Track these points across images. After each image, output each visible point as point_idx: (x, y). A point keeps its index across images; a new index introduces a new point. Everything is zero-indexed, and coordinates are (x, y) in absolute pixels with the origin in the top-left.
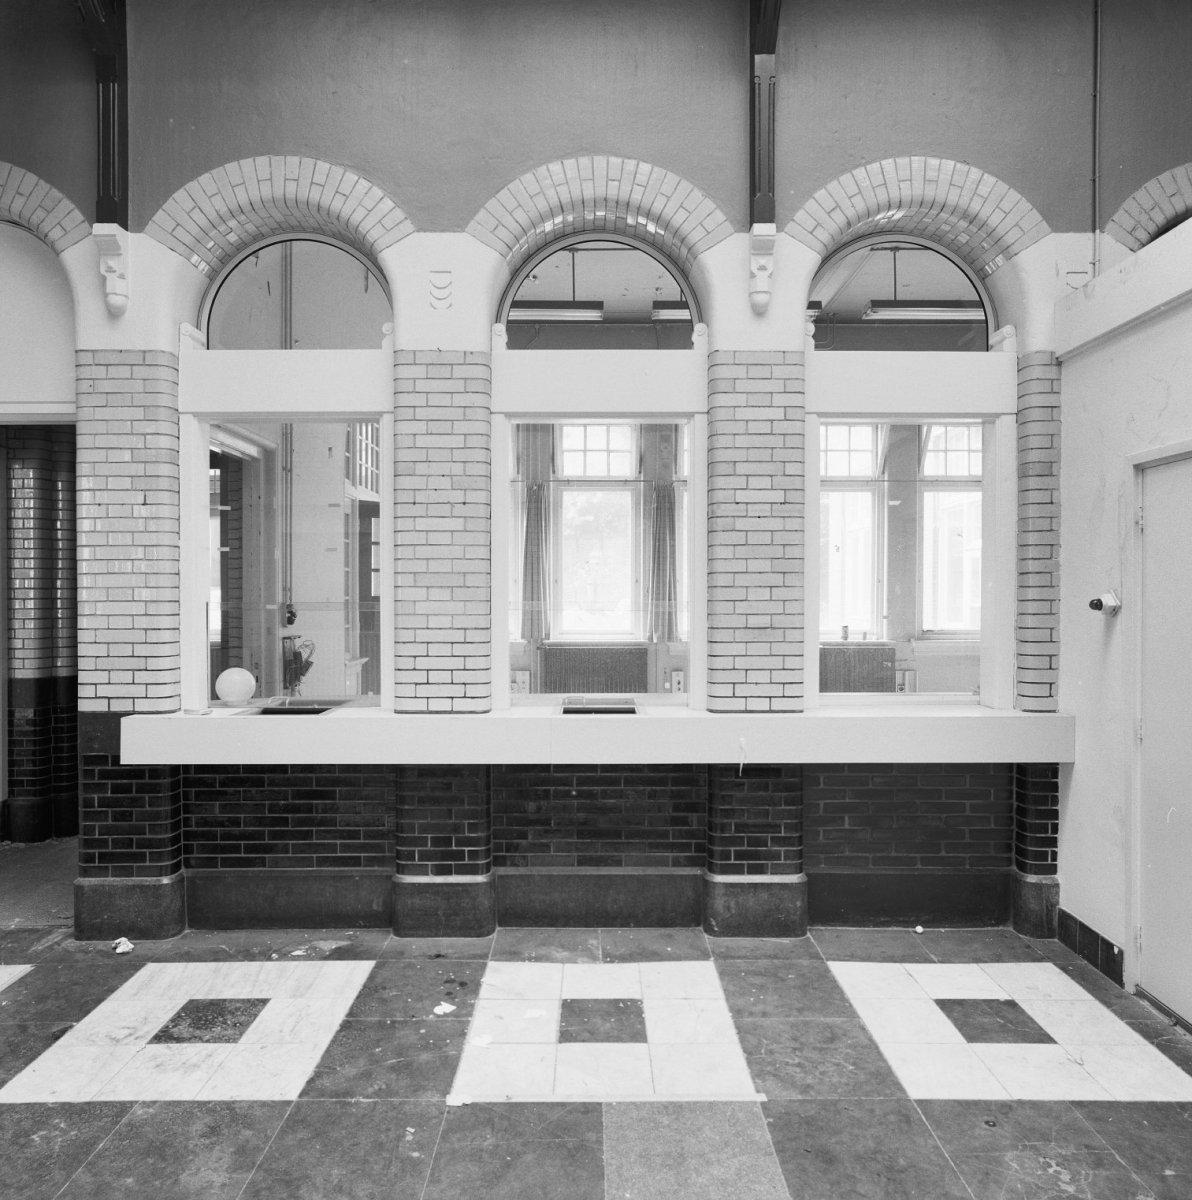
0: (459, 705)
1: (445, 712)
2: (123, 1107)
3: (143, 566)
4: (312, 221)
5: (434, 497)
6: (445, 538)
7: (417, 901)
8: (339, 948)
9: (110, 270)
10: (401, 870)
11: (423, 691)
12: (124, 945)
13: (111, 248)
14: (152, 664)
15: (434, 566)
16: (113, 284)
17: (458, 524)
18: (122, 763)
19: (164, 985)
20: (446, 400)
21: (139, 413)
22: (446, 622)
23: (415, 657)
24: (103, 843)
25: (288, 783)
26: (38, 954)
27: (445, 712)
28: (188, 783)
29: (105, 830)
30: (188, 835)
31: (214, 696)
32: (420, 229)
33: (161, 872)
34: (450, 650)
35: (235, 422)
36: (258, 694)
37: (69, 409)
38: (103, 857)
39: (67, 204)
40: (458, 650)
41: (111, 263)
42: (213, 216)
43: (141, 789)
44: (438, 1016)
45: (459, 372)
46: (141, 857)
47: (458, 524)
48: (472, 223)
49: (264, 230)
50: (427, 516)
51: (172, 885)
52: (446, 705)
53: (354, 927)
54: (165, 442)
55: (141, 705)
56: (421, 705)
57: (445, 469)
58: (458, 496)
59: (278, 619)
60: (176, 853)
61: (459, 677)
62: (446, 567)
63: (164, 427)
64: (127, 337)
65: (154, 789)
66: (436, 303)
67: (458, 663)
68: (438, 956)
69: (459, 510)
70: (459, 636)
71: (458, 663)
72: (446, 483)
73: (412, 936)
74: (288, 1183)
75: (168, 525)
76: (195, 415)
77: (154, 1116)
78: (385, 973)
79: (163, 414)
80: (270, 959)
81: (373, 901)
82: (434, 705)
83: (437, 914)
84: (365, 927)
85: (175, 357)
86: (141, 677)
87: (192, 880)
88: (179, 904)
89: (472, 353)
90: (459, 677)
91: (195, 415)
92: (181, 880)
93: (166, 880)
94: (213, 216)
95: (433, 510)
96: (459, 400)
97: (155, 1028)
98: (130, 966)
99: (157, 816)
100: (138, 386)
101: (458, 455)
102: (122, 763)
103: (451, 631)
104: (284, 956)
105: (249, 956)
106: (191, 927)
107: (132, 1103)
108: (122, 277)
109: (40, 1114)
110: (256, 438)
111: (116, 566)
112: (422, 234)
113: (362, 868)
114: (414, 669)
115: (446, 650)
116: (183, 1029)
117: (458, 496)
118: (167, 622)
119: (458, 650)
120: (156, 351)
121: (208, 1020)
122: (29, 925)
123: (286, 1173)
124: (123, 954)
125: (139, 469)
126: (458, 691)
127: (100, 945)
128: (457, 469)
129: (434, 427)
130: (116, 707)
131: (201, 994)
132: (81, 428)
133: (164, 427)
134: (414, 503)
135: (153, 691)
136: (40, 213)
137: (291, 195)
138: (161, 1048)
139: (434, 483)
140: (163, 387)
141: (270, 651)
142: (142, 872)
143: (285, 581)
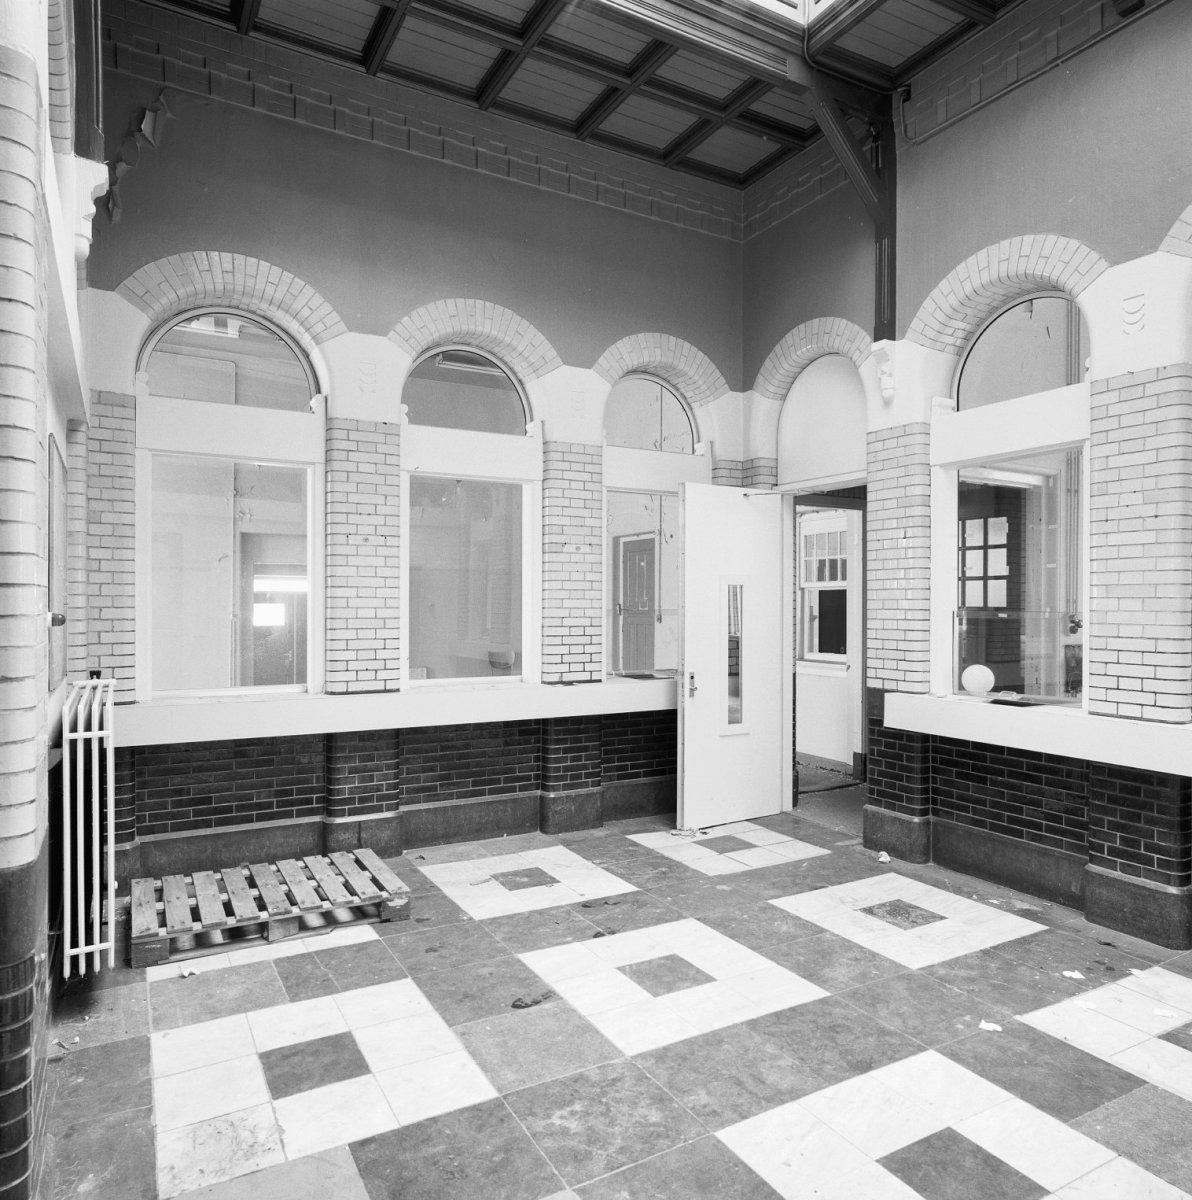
0: (1149, 713)
1: (1135, 718)
2: (822, 930)
3: (903, 583)
4: (1012, 289)
5: (1128, 513)
6: (1138, 551)
7: (1104, 892)
8: (1029, 910)
9: (883, 373)
10: (1093, 860)
11: (1113, 695)
12: (884, 857)
13: (883, 357)
14: (909, 656)
15: (1125, 579)
16: (886, 382)
17: (1150, 537)
18: (885, 725)
19: (896, 885)
20: (1139, 418)
21: (901, 472)
22: (1137, 631)
23: (1106, 663)
24: (879, 783)
25: (972, 756)
26: (838, 847)
27: (1135, 718)
28: (936, 750)
29: (881, 774)
30: (936, 791)
31: (961, 687)
32: (1114, 263)
33: (912, 812)
34: (1140, 659)
35: (1004, 461)
36: (996, 689)
37: (863, 474)
38: (880, 793)
39: (863, 333)
40: (1149, 659)
41: (884, 368)
42: (949, 311)
43: (903, 748)
44: (1064, 977)
45: (1151, 389)
46: (900, 798)
47: (1150, 537)
48: (1167, 239)
49: (995, 304)
50: (1119, 532)
51: (919, 824)
52: (1136, 711)
53: (1054, 901)
54: (919, 490)
55: (902, 686)
56: (1111, 709)
57: (1137, 485)
58: (1151, 510)
59: (1059, 627)
60: (926, 801)
61: (1149, 685)
62: (1138, 578)
63: (917, 480)
64: (896, 417)
65: (910, 749)
66: (1129, 328)
67: (1149, 672)
68: (1108, 944)
69: (1151, 523)
70: (1150, 646)
71: (1149, 672)
72: (1138, 498)
73: (1099, 924)
74: (874, 999)
75: (920, 552)
76: (941, 466)
77: (833, 941)
78: (1048, 937)
79: (917, 469)
80: (970, 897)
81: (1071, 883)
82: (1124, 710)
83: (1122, 910)
84: (1064, 904)
85: (927, 425)
86: (903, 665)
87: (936, 825)
88: (924, 841)
89: (1165, 368)
90: (1149, 685)
91: (941, 466)
92: (928, 823)
93: (916, 820)
94: (949, 311)
95: (1124, 525)
96: (1151, 416)
97: (866, 905)
98: (878, 869)
99: (910, 770)
100: (380, 561)
101: (1150, 470)
102: (885, 725)
103: (1142, 640)
104: (982, 899)
105: (958, 891)
106: (934, 861)
107: (827, 931)
108: (890, 375)
109: (786, 916)
110: (1037, 469)
111: (888, 584)
112: (1116, 268)
113: (1063, 851)
114: (1105, 675)
115: (1137, 658)
116: (880, 912)
117: (1151, 510)
118: (918, 625)
119: (1149, 659)
120: (911, 424)
121: (899, 912)
122: (846, 831)
123: (878, 995)
124: (882, 862)
125: (901, 513)
126: (1149, 699)
127: (873, 853)
128: (1150, 483)
129: (1126, 447)
130: (888, 685)
131: (907, 899)
132: (869, 489)
133: (917, 480)
134: (1107, 521)
135: (910, 676)
136: (848, 344)
137: (1003, 274)
138: (863, 915)
139: (1126, 499)
140: (918, 449)
141: (1051, 657)
142: (902, 810)
143: (1068, 594)
